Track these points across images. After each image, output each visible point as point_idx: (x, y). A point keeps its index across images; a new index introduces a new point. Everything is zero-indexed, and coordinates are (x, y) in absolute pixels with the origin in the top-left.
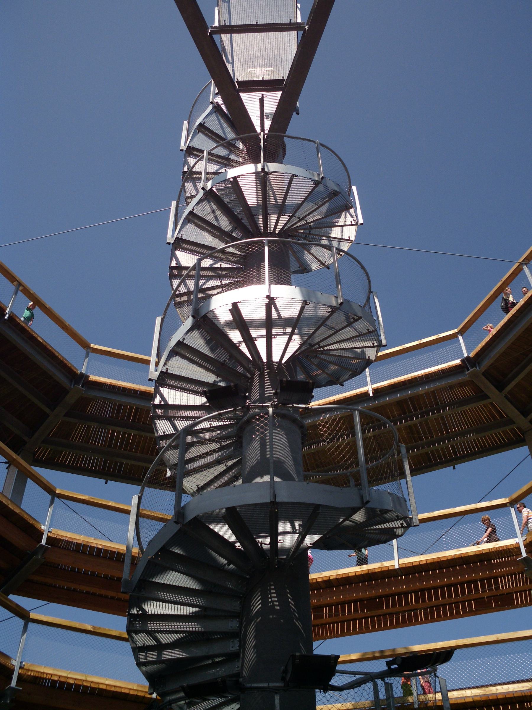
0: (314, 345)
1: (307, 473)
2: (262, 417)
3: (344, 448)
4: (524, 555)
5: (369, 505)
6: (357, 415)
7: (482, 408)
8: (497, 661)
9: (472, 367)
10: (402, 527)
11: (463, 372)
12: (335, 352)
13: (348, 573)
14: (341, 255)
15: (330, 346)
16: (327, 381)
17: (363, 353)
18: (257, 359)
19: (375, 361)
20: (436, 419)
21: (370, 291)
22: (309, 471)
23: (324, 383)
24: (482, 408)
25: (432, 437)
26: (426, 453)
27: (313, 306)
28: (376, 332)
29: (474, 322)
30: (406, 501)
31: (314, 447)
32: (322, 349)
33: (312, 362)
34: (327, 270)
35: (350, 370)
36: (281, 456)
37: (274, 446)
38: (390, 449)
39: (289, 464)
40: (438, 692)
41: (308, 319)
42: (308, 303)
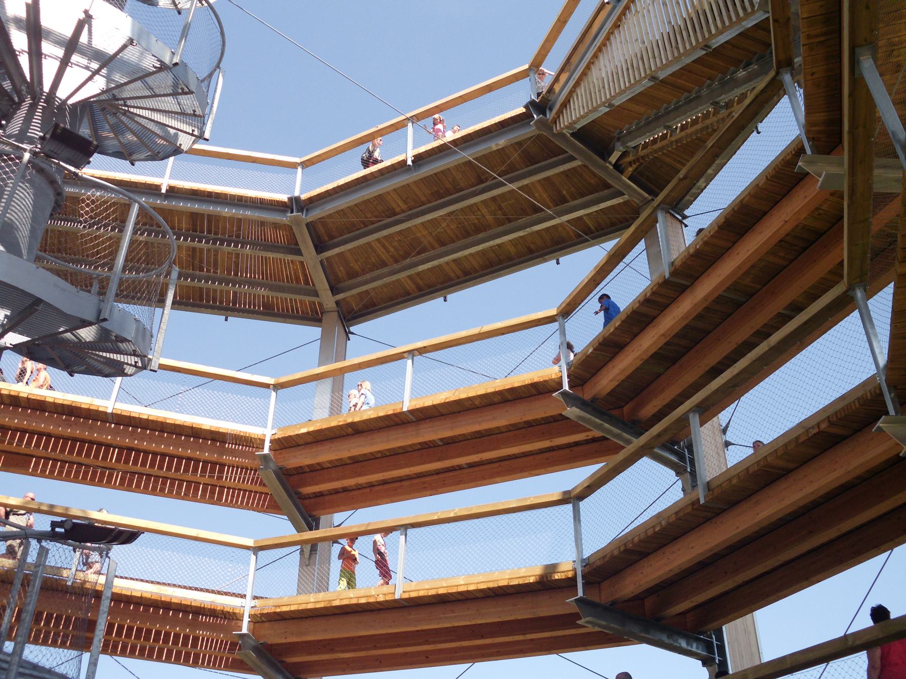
0: (118, 100)
1: (42, 254)
2: (11, 159)
3: (103, 242)
4: (266, 450)
5: (104, 324)
6: (135, 209)
7: (288, 263)
8: (187, 560)
9: (298, 211)
10: (135, 366)
11: (285, 211)
12: (142, 119)
13: (45, 397)
14: (203, 5)
15: (138, 110)
16: (116, 150)
17: (176, 135)
18: (36, 84)
19: (186, 152)
20: (228, 253)
21: (218, 66)
22: (45, 251)
23: (110, 152)
24: (288, 263)
25: (215, 272)
26: (200, 287)
27: (139, 51)
28: (202, 119)
29: (324, 160)
30: (152, 336)
31: (54, 223)
32: (126, 108)
33: (106, 119)
34: (177, 13)
35: (150, 150)
36: (16, 219)
37: (13, 203)
38: (159, 266)
39: (23, 234)
40: (103, 574)
41: (124, 63)
42: (135, 44)
